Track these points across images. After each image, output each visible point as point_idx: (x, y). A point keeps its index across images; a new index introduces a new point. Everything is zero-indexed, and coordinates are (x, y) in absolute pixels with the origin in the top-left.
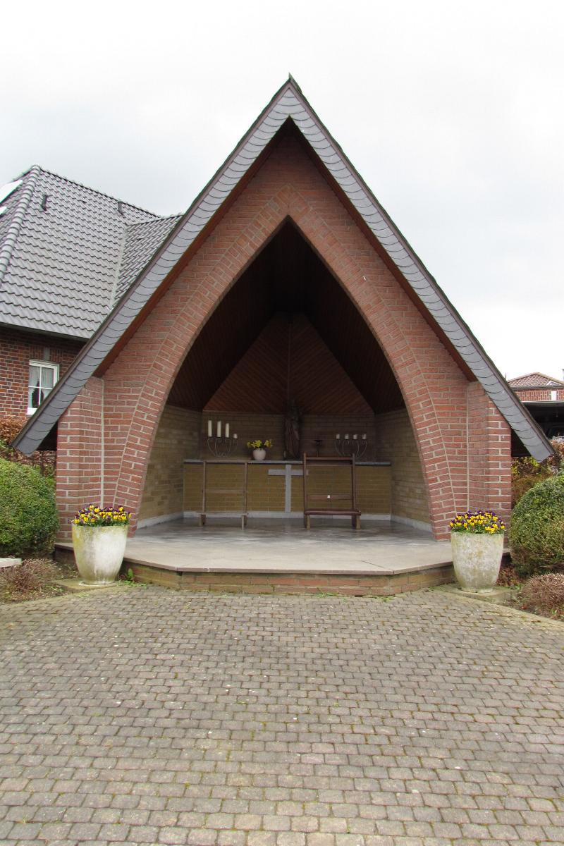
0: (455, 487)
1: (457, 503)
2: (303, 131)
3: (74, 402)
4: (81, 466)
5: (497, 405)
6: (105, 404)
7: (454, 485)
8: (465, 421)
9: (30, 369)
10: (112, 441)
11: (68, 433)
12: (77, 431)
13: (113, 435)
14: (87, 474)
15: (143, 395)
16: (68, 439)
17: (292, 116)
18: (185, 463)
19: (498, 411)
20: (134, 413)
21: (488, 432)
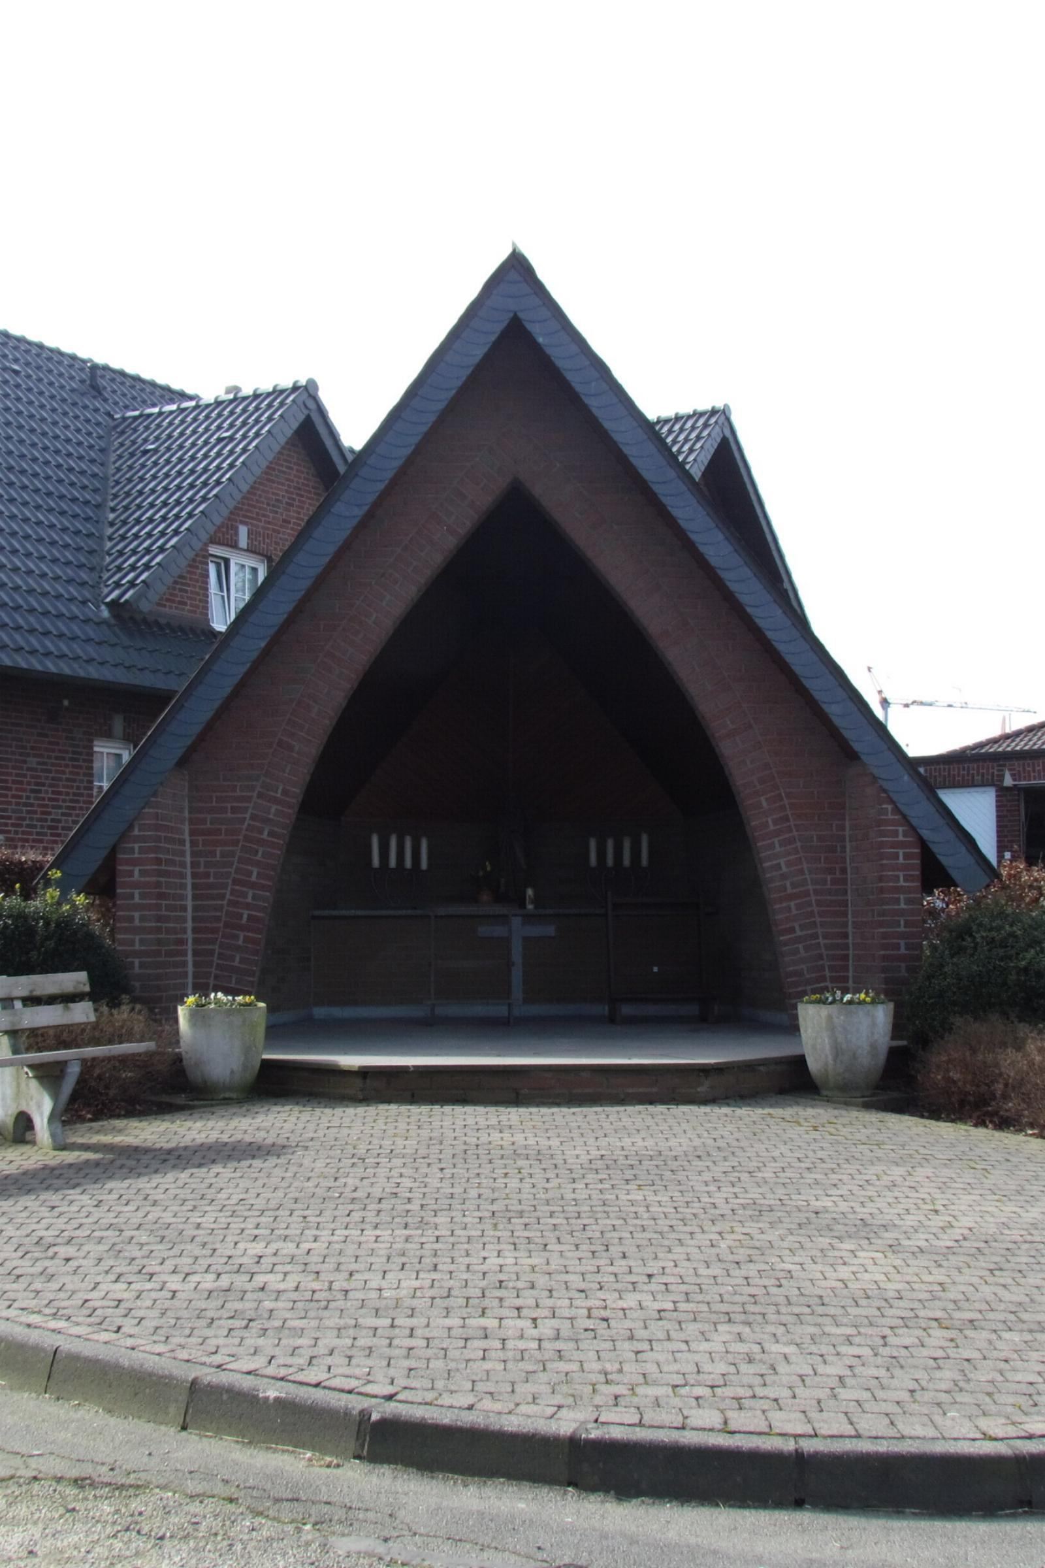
0: (826, 941)
1: (831, 968)
2: (540, 340)
3: (146, 810)
4: (159, 919)
5: (895, 799)
6: (190, 812)
7: (825, 937)
8: (843, 828)
9: (95, 755)
10: (207, 875)
11: (135, 862)
12: (152, 858)
13: (207, 864)
14: (168, 931)
15: (260, 795)
16: (136, 873)
17: (521, 315)
18: (314, 917)
19: (897, 810)
20: (244, 827)
21: (882, 845)
